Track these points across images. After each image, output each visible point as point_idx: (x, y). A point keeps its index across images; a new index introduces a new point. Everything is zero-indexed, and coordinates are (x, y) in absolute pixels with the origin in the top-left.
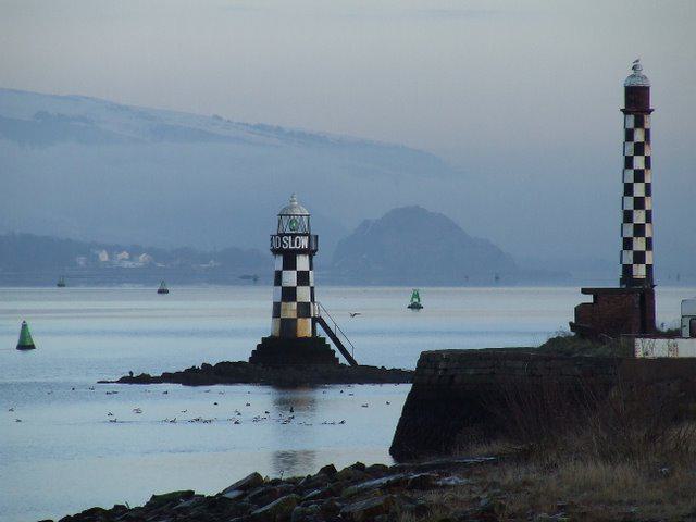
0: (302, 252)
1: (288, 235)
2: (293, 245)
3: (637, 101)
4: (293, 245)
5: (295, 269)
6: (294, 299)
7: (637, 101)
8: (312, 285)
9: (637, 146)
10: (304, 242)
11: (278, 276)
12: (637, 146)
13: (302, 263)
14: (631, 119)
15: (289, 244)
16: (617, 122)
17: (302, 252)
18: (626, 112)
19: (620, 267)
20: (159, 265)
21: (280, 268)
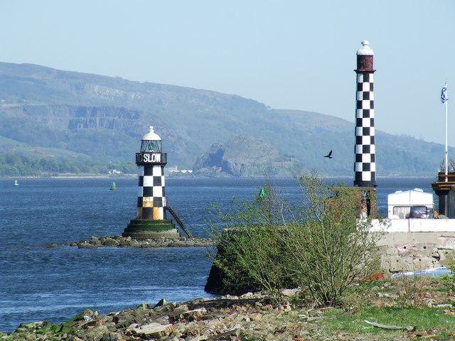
0: (156, 164)
1: (148, 153)
2: (151, 159)
3: (364, 65)
4: (151, 159)
5: (152, 196)
6: (155, 185)
7: (364, 65)
8: (163, 185)
9: (362, 95)
10: (158, 158)
11: (141, 179)
12: (362, 95)
13: (157, 171)
14: (362, 77)
15: (147, 159)
16: (352, 78)
17: (156, 164)
18: (358, 72)
19: (354, 173)
20: (184, 171)
21: (371, 93)
